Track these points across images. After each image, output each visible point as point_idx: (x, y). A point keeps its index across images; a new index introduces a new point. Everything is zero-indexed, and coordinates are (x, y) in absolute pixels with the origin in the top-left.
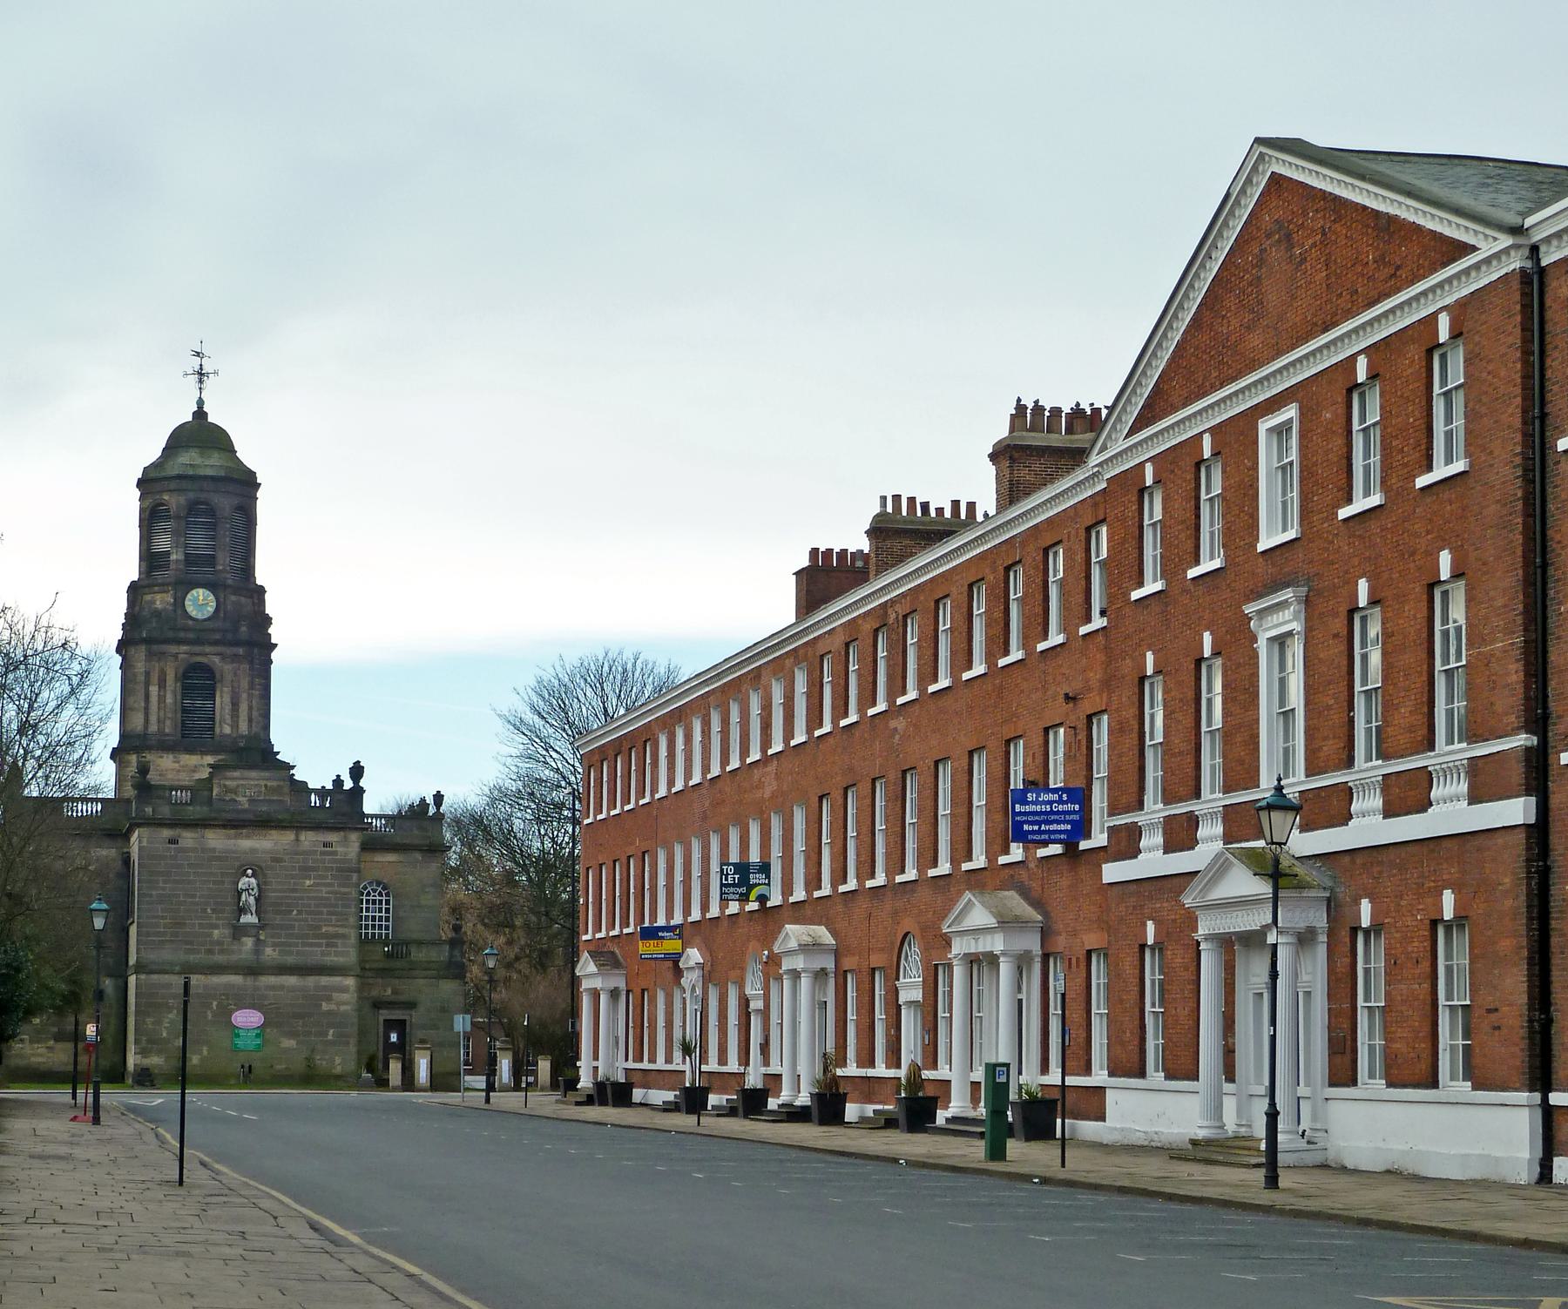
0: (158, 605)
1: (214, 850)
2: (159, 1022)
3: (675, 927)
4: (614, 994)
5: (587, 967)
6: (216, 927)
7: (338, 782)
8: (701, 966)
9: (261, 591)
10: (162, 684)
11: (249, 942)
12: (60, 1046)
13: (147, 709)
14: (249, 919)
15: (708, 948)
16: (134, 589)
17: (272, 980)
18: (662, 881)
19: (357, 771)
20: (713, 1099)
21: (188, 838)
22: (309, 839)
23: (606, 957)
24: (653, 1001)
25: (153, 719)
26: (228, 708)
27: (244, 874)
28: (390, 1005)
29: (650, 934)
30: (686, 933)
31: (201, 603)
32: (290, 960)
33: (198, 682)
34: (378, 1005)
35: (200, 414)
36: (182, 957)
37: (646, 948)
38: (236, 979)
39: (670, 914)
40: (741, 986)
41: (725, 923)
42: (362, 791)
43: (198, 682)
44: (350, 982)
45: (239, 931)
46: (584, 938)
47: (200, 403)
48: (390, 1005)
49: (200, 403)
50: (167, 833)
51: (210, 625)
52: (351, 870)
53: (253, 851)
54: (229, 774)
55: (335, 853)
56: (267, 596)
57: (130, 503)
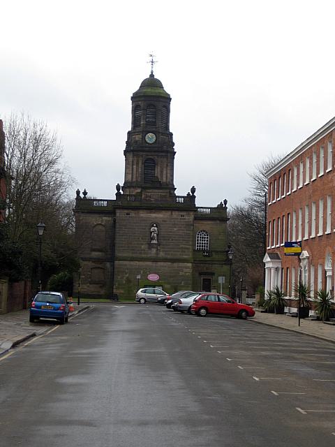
0: (137, 139)
1: (142, 217)
2: (122, 278)
3: (299, 242)
4: (277, 269)
5: (267, 259)
6: (142, 244)
7: (189, 194)
8: (308, 258)
9: (172, 134)
10: (137, 164)
11: (154, 250)
12: (91, 286)
13: (132, 173)
14: (154, 242)
15: (311, 251)
16: (129, 133)
17: (162, 264)
18: (294, 225)
19: (193, 190)
20: (311, 313)
21: (133, 214)
22: (176, 214)
23: (274, 256)
24: (291, 272)
25: (134, 177)
26: (159, 173)
27: (153, 226)
28: (205, 274)
29: (289, 245)
30: (303, 245)
31: (151, 138)
32: (169, 257)
33: (150, 164)
34: (200, 274)
35: (152, 75)
36: (131, 255)
37: (288, 250)
38: (149, 263)
39: (297, 238)
40: (323, 265)
41: (319, 180)
42: (195, 197)
43: (150, 164)
44: (190, 265)
45: (151, 246)
46: (268, 248)
47: (152, 72)
48: (205, 274)
49: (152, 72)
50: (126, 211)
51: (153, 145)
52: (191, 225)
53: (156, 217)
54: (148, 191)
55: (185, 219)
56: (173, 136)
57: (129, 106)
